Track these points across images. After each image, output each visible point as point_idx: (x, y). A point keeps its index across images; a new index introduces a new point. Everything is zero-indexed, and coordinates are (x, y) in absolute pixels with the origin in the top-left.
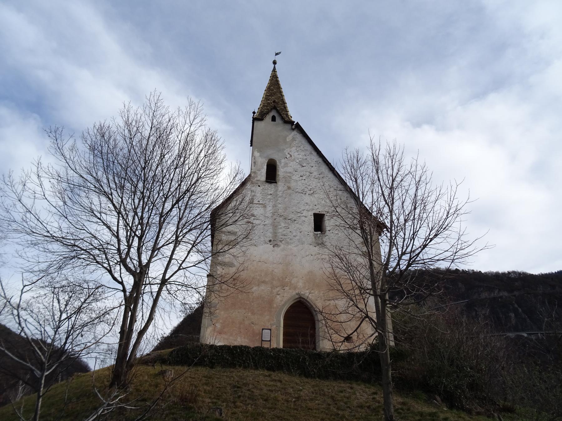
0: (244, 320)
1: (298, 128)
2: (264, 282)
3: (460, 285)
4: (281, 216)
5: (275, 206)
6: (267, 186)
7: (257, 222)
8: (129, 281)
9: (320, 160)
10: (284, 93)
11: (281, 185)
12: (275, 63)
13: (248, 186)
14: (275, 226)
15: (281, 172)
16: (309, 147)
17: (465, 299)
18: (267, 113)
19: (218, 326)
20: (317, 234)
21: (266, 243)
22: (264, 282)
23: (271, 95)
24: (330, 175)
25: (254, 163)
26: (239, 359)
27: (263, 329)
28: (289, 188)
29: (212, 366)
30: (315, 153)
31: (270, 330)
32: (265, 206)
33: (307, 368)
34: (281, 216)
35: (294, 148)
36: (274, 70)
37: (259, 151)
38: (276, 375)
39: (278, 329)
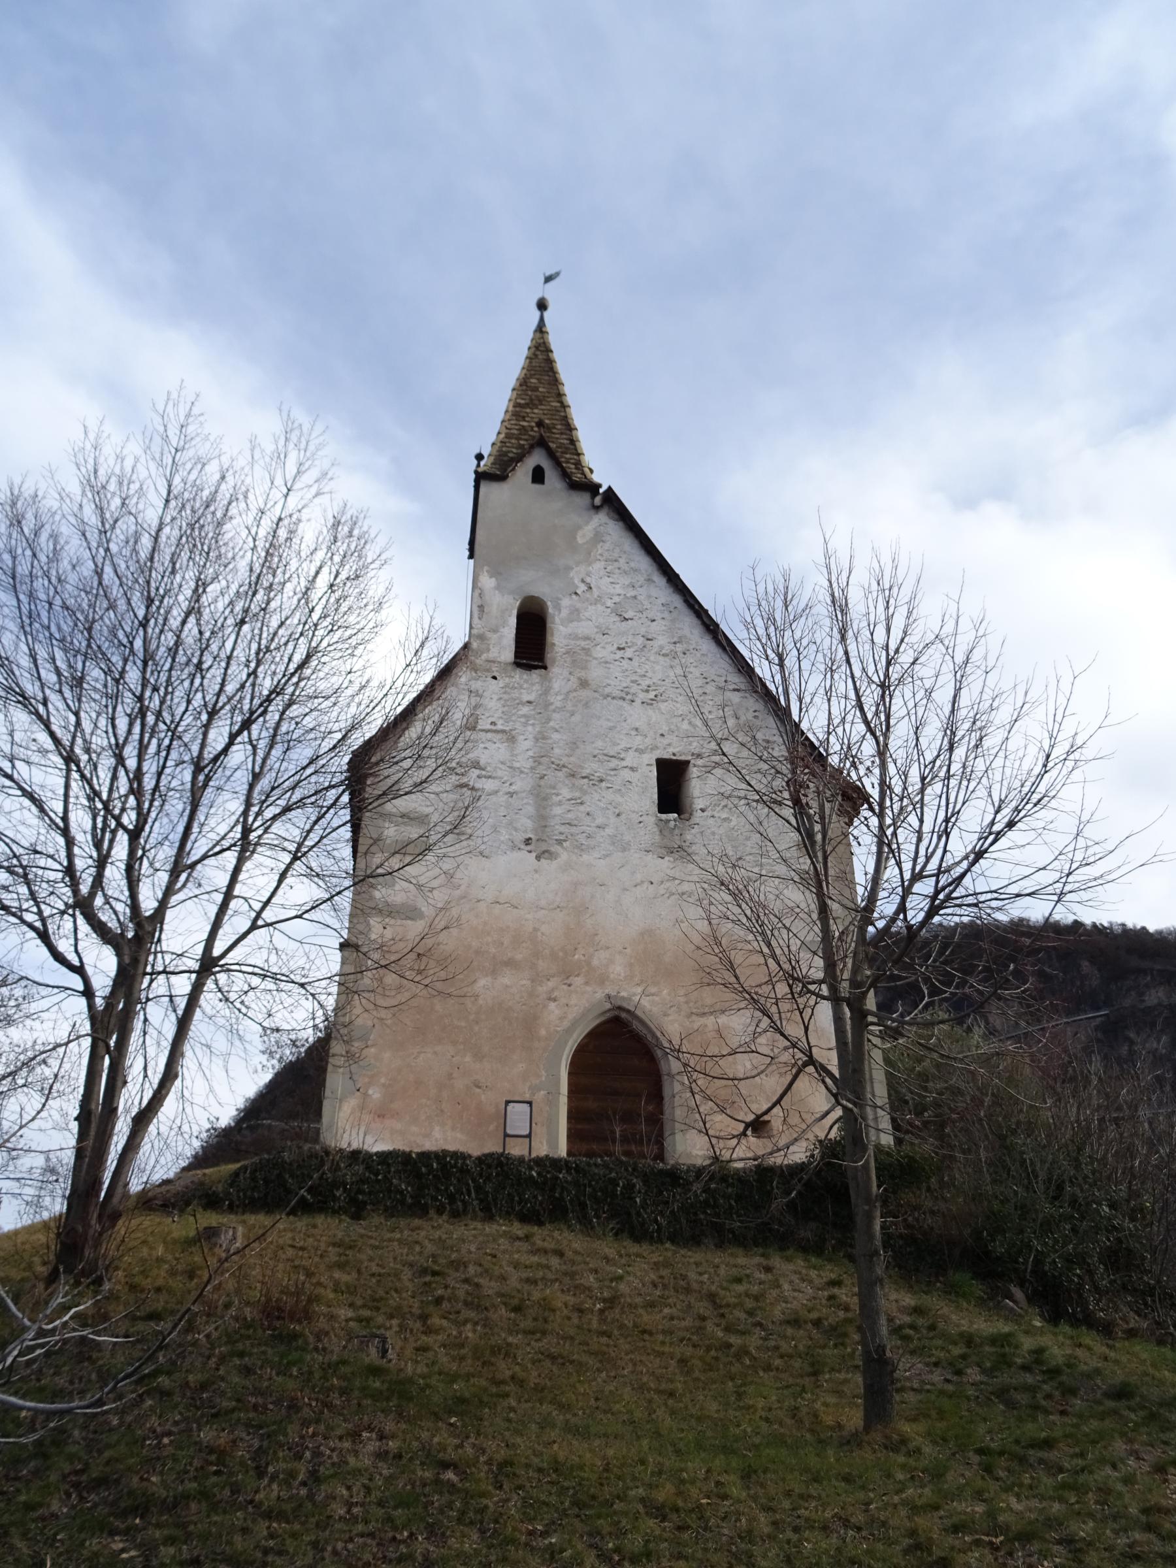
0: (450, 1076)
1: (612, 503)
2: (510, 963)
3: (1085, 965)
4: (560, 767)
5: (540, 737)
6: (519, 676)
7: (489, 785)
8: (103, 964)
9: (677, 601)
10: (570, 399)
11: (560, 675)
12: (542, 305)
13: (463, 677)
14: (542, 798)
15: (560, 635)
16: (643, 562)
17: (1098, 1009)
18: (520, 458)
19: (375, 1094)
20: (668, 821)
21: (514, 847)
22: (510, 963)
23: (531, 404)
24: (707, 645)
25: (480, 608)
26: (438, 1190)
27: (508, 1102)
28: (584, 684)
29: (356, 1211)
30: (661, 581)
31: (530, 1103)
32: (510, 738)
33: (639, 1214)
34: (560, 767)
35: (598, 566)
36: (541, 329)
37: (495, 573)
38: (543, 1236)
39: (553, 1094)
